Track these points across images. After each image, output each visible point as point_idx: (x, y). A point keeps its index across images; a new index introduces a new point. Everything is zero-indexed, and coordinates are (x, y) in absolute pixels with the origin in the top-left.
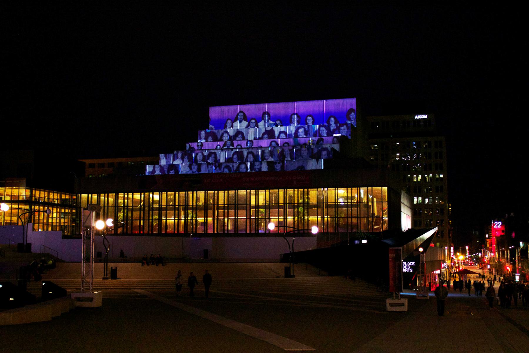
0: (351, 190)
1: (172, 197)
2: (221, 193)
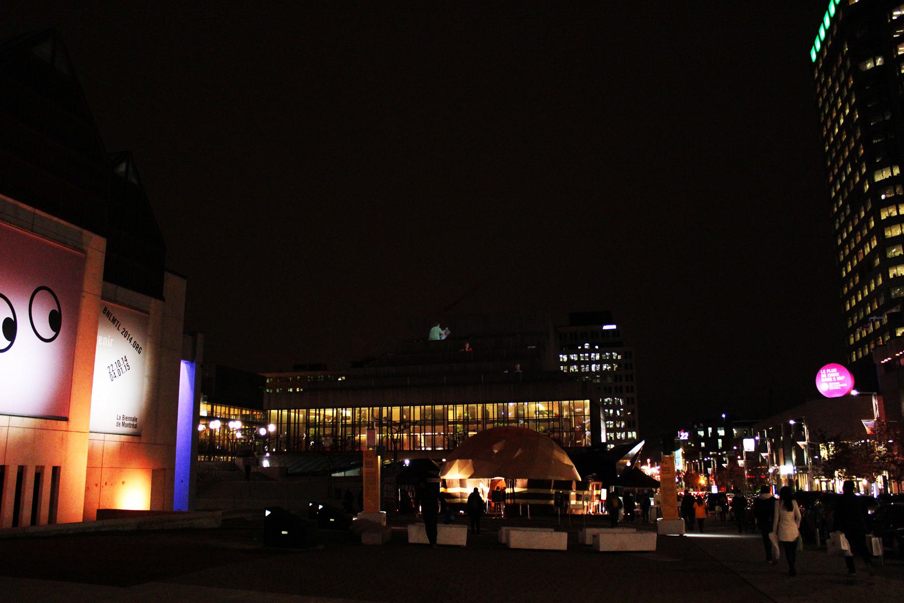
2: (417, 408)
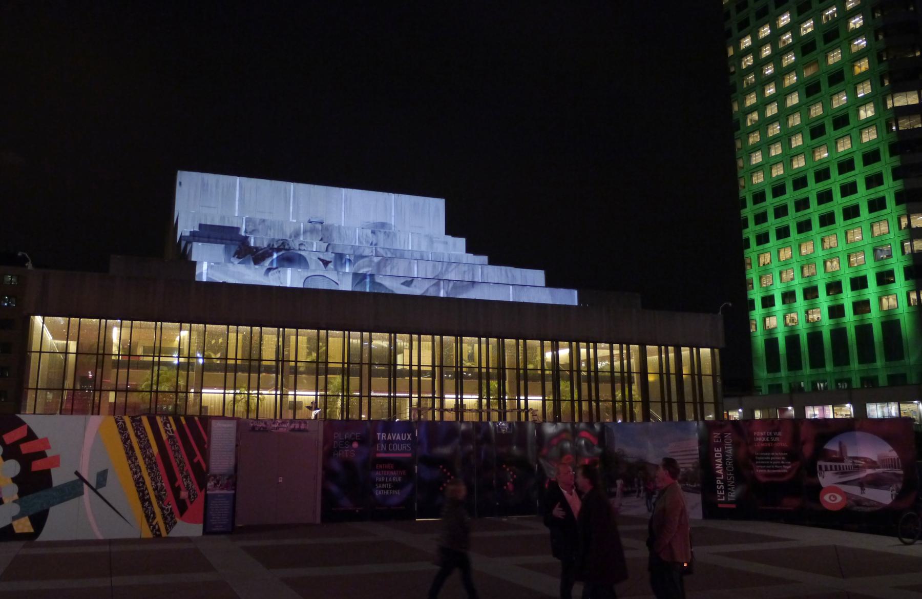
0: (419, 341)
1: (220, 340)
